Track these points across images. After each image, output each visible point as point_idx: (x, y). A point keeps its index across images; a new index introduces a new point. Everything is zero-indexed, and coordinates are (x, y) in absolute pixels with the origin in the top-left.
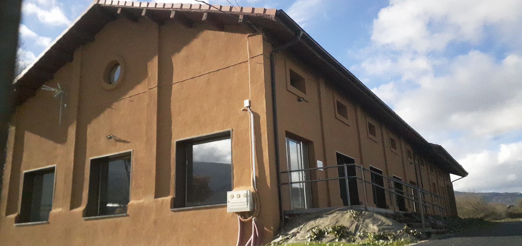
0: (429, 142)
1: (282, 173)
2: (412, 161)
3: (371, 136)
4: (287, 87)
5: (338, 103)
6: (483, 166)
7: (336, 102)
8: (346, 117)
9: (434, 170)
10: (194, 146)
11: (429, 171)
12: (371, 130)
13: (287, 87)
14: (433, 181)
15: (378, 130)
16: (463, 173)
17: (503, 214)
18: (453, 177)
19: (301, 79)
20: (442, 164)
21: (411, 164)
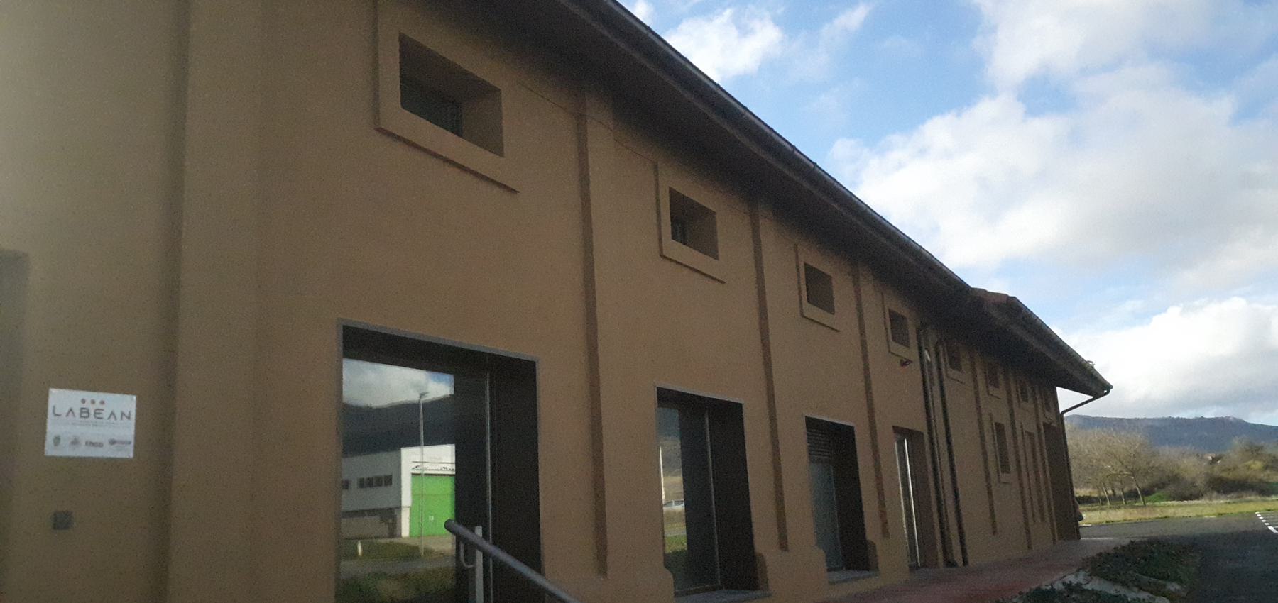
0: (973, 285)
1: (1029, 547)
2: (913, 354)
3: (814, 312)
4: (376, 111)
5: (674, 195)
6: (1151, 357)
7: (802, 265)
8: (710, 249)
9: (1001, 378)
10: (131, 455)
11: (981, 387)
12: (817, 289)
13: (376, 111)
14: (997, 419)
15: (841, 288)
16: (1094, 385)
17: (1200, 483)
18: (1066, 398)
19: (705, 214)
20: (1010, 350)
21: (904, 364)
